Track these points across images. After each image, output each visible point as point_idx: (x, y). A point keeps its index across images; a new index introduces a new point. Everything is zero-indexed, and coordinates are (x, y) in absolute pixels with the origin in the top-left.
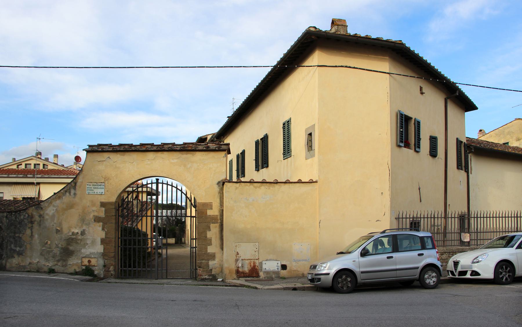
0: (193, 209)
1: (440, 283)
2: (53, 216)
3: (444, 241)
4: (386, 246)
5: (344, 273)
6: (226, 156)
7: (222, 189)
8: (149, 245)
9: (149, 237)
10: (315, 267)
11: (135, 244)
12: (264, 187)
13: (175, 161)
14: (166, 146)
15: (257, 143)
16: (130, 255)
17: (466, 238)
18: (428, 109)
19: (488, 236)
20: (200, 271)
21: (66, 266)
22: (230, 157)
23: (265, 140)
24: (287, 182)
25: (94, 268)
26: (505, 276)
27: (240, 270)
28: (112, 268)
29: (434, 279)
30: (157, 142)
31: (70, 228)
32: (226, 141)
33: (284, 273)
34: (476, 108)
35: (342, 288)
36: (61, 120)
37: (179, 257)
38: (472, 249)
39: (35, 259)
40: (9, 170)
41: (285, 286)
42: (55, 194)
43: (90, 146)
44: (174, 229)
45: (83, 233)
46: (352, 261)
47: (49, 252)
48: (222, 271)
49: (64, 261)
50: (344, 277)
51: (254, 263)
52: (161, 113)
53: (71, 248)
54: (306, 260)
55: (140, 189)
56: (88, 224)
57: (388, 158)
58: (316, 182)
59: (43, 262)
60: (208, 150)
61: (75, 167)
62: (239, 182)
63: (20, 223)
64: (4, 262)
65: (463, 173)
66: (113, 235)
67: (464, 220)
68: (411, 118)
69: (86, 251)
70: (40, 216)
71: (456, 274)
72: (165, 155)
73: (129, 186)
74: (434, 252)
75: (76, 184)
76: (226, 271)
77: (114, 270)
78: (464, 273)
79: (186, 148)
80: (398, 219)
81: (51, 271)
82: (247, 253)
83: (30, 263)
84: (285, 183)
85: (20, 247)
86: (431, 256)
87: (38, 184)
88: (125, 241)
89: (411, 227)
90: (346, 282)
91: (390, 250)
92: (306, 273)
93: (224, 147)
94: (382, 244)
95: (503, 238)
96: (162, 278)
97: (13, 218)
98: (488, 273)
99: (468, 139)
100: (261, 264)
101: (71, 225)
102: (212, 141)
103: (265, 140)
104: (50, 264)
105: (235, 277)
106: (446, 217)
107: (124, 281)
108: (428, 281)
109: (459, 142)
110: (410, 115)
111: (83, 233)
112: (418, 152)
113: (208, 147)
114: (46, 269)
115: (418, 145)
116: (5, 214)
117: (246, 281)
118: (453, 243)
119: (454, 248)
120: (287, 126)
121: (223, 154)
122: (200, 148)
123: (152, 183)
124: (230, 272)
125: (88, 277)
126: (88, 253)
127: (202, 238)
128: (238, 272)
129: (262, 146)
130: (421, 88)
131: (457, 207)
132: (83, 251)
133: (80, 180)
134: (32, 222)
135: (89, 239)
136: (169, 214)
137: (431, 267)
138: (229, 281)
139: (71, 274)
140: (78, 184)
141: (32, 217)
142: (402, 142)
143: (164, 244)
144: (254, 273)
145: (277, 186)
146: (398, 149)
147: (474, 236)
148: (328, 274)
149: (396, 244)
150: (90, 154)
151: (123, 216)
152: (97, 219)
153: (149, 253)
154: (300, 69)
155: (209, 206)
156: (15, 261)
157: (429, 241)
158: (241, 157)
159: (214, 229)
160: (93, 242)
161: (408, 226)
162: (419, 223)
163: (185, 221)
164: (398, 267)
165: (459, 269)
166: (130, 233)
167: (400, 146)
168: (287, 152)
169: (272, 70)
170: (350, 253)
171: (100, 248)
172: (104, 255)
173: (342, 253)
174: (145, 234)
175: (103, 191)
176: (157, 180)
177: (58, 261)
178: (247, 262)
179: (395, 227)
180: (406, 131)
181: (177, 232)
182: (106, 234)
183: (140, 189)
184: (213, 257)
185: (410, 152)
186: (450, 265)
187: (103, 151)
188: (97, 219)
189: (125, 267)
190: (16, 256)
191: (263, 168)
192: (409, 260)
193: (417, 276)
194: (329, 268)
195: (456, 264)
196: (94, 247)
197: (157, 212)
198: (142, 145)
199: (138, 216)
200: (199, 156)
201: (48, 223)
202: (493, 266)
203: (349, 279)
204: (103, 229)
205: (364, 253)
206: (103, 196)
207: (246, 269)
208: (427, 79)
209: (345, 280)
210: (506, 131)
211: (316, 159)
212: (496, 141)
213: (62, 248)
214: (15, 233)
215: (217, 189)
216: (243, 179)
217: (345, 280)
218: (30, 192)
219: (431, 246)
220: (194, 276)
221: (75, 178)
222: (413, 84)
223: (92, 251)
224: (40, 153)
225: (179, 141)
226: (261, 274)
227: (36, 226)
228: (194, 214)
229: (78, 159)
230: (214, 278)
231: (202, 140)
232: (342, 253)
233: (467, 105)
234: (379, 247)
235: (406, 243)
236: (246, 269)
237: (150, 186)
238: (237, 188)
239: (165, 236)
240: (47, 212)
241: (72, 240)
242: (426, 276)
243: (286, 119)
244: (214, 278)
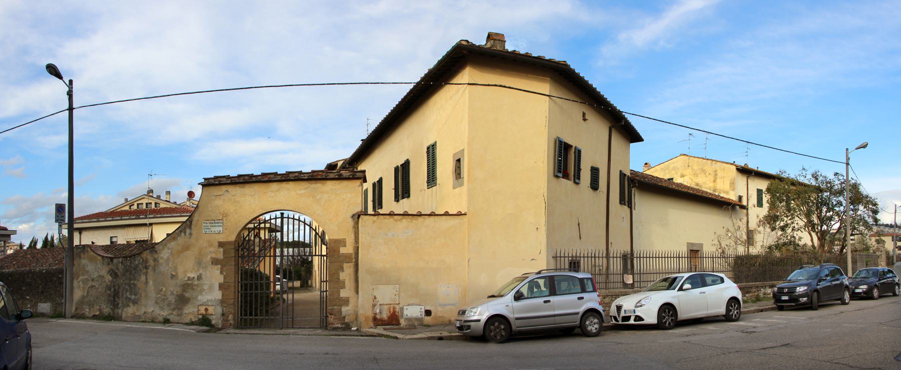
0: (324, 247)
1: (604, 329)
2: (168, 259)
3: (606, 283)
4: (543, 288)
5: (496, 319)
6: (362, 185)
7: (357, 223)
8: (272, 290)
9: (272, 280)
10: (464, 312)
11: (256, 289)
12: (405, 221)
13: (303, 191)
14: (291, 175)
15: (396, 169)
16: (251, 301)
17: (629, 280)
18: (591, 138)
19: (651, 277)
20: (331, 319)
21: (180, 315)
22: (365, 186)
23: (406, 166)
24: (432, 214)
25: (211, 317)
26: (668, 320)
27: (378, 317)
28: (231, 317)
29: (596, 326)
30: (282, 171)
31: (185, 272)
32: (360, 168)
33: (428, 320)
34: (642, 140)
35: (495, 336)
36: (175, 153)
37: (306, 303)
38: (635, 292)
39: (149, 307)
40: (122, 211)
41: (429, 335)
42: (168, 235)
43: (205, 179)
44: (299, 270)
45: (199, 278)
46: (504, 306)
47: (164, 300)
48: (356, 319)
49: (179, 309)
50: (496, 324)
51: (394, 308)
52: (285, 139)
53: (187, 295)
54: (453, 305)
55: (262, 226)
56: (205, 268)
57: (544, 190)
58: (465, 214)
59: (158, 311)
60: (340, 178)
61: (188, 203)
62: (377, 214)
63: (135, 269)
64: (120, 311)
65: (626, 208)
66: (232, 279)
67: (628, 259)
68: (571, 146)
69: (203, 298)
70: (155, 260)
71: (620, 319)
72: (291, 185)
73: (250, 222)
74: (595, 295)
75: (191, 222)
76: (361, 319)
77: (234, 319)
78: (627, 318)
79: (314, 177)
80: (555, 257)
81: (166, 321)
82: (386, 296)
83: (145, 313)
84: (430, 215)
85: (135, 295)
86: (592, 301)
87: (151, 224)
88: (246, 285)
89: (570, 267)
90: (499, 329)
91: (547, 294)
92: (453, 319)
93: (359, 175)
94: (538, 286)
95: (665, 280)
96: (288, 328)
97: (129, 264)
98: (651, 318)
99: (633, 173)
100: (402, 309)
101: (187, 269)
102: (343, 167)
103: (406, 166)
104: (165, 313)
105: (372, 324)
106: (608, 256)
107: (244, 331)
108: (589, 328)
109: (622, 175)
110: (570, 143)
111: (199, 278)
112: (577, 184)
113: (341, 175)
114: (161, 319)
115: (577, 178)
116: (121, 260)
117: (385, 329)
118: (616, 285)
119: (617, 291)
120: (431, 151)
121: (358, 182)
122: (332, 176)
123: (276, 218)
124: (366, 318)
125: (205, 328)
126: (205, 300)
127: (333, 279)
128: (375, 319)
129: (403, 172)
130: (584, 114)
131: (620, 245)
132: (200, 298)
133: (195, 218)
134: (147, 268)
135: (206, 282)
136: (291, 253)
137: (592, 312)
138: (365, 330)
139: (187, 324)
140: (194, 223)
141: (146, 261)
142: (560, 172)
143: (290, 288)
144: (393, 320)
145: (420, 219)
146: (555, 180)
147: (637, 278)
148: (479, 321)
149: (553, 286)
150: (206, 188)
151: (243, 257)
152: (215, 262)
153: (273, 299)
154: (448, 86)
155: (342, 242)
156: (130, 310)
157: (590, 283)
158: (378, 186)
159: (348, 269)
160: (211, 287)
161: (567, 267)
162: (579, 263)
163: (312, 261)
164: (556, 312)
165: (622, 314)
166: (251, 275)
167: (557, 177)
168: (432, 179)
169: (415, 87)
170: (502, 296)
171: (217, 295)
172: (222, 302)
173: (493, 296)
174: (268, 278)
175: (221, 229)
176: (282, 214)
177: (173, 310)
178: (386, 307)
179: (553, 267)
180: (565, 160)
181: (303, 273)
182: (225, 278)
183: (262, 226)
184: (346, 302)
185: (569, 183)
186: (613, 310)
187: (220, 184)
188: (215, 262)
189: (246, 315)
190: (131, 305)
191: (403, 198)
192: (568, 305)
193: (578, 323)
194: (480, 314)
195: (619, 308)
196: (212, 292)
197: (282, 252)
198: (264, 175)
199: (259, 257)
200: (330, 185)
201: (163, 268)
202: (656, 310)
203: (503, 327)
204: (221, 273)
205: (518, 297)
206: (221, 236)
207: (385, 316)
208: (591, 105)
209: (498, 327)
210: (671, 166)
211: (465, 188)
212: (661, 177)
213: (177, 295)
214: (130, 280)
215: (351, 223)
216: (380, 211)
217: (498, 327)
218: (142, 234)
219: (591, 289)
220: (324, 325)
221: (190, 216)
222: (576, 108)
223: (209, 297)
224: (152, 191)
225: (307, 169)
226: (402, 322)
227: (150, 271)
228: (324, 253)
229: (191, 194)
230: (347, 327)
231: (331, 167)
232: (493, 296)
233: (633, 136)
234: (535, 290)
235: (564, 285)
236: (385, 316)
237: (273, 221)
238: (374, 222)
239: (290, 279)
240: (162, 255)
241: (187, 286)
242: (588, 323)
243: (431, 142)
244: (347, 327)
